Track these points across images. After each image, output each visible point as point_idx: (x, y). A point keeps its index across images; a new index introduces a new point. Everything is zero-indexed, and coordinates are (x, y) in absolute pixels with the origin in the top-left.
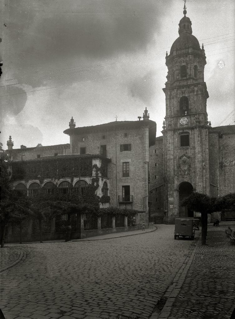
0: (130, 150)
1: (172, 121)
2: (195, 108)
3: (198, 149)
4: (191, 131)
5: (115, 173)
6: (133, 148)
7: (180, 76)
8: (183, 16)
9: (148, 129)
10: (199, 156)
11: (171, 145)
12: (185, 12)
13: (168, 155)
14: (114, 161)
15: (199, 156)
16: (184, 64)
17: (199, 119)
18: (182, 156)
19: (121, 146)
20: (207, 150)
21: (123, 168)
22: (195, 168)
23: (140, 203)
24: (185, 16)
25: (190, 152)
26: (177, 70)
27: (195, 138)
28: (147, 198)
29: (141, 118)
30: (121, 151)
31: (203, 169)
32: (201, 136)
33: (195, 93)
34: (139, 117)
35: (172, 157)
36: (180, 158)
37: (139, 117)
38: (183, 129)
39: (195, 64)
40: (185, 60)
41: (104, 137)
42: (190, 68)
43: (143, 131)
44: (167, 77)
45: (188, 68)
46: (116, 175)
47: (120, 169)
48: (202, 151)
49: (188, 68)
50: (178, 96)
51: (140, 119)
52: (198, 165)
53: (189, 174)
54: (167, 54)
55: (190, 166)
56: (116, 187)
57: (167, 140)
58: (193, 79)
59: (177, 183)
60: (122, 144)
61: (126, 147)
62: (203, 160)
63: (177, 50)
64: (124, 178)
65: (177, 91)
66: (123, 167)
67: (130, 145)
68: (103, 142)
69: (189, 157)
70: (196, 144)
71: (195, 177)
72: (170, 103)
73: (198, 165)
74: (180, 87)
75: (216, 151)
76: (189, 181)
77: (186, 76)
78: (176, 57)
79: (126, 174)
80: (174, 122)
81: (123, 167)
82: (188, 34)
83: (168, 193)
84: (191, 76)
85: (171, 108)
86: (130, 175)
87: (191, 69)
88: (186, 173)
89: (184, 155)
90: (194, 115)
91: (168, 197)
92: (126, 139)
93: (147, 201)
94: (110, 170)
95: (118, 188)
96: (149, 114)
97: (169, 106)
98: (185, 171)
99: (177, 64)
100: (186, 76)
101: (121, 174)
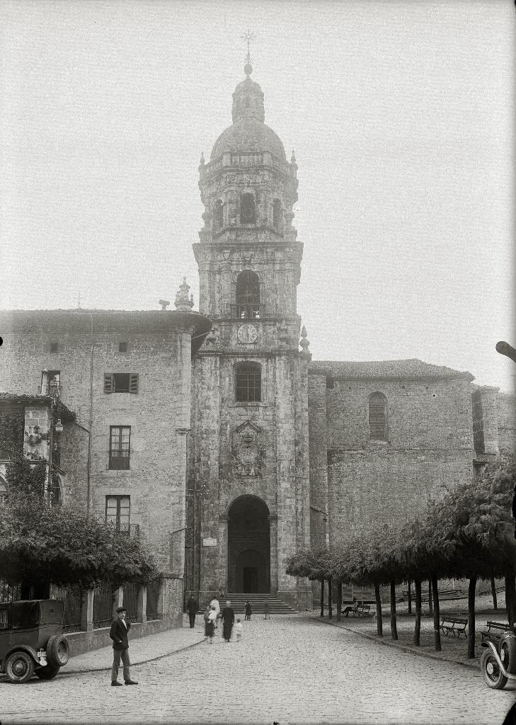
0: (135, 390)
1: (217, 330)
2: (276, 305)
3: (284, 410)
4: (267, 361)
5: (86, 455)
6: (143, 383)
7: (238, 219)
8: (242, 77)
9: (189, 337)
10: (286, 428)
11: (210, 393)
12: (248, 70)
13: (205, 421)
14: (82, 419)
15: (286, 428)
16: (247, 191)
17: (287, 333)
18: (243, 426)
19: (107, 377)
20: (306, 414)
21: (111, 443)
22: (277, 460)
23: (160, 551)
24: (248, 79)
25: (262, 417)
26: (231, 202)
27: (278, 380)
28: (183, 534)
29: (168, 303)
30: (108, 393)
31: (297, 462)
32: (292, 375)
33: (277, 267)
34: (161, 302)
35: (216, 427)
36: (238, 430)
37: (161, 302)
38: (245, 355)
39: (276, 196)
40: (251, 181)
41: (54, 348)
42: (265, 202)
43: (176, 341)
44: (204, 217)
45: (259, 202)
46: (89, 463)
47: (101, 446)
48: (296, 416)
49: (259, 202)
50: (234, 268)
51: (164, 307)
52: (285, 451)
53: (258, 475)
54: (202, 161)
55: (262, 454)
56: (88, 499)
57: (203, 378)
58: (272, 231)
59: (226, 499)
60: (110, 371)
61: (122, 383)
62: (295, 440)
63: (232, 154)
64: (113, 473)
65: (231, 253)
66: (111, 439)
67: (136, 377)
68: (52, 363)
69: (259, 430)
70: (280, 395)
71: (276, 482)
72: (212, 283)
73: (285, 451)
74: (237, 247)
75: (321, 420)
76: (260, 495)
77: (253, 221)
78: (230, 171)
79: (119, 461)
80: (221, 334)
81: (111, 439)
82: (258, 123)
83: (202, 523)
84: (268, 224)
85: (212, 297)
86: (131, 465)
87: (266, 206)
88: (252, 471)
89: (248, 423)
90: (275, 321)
91: (202, 535)
92: (123, 358)
93: (183, 544)
94: (70, 446)
95: (91, 504)
96: (192, 296)
97: (210, 291)
98: (247, 466)
99: (232, 188)
100: (253, 221)
101: (104, 461)
